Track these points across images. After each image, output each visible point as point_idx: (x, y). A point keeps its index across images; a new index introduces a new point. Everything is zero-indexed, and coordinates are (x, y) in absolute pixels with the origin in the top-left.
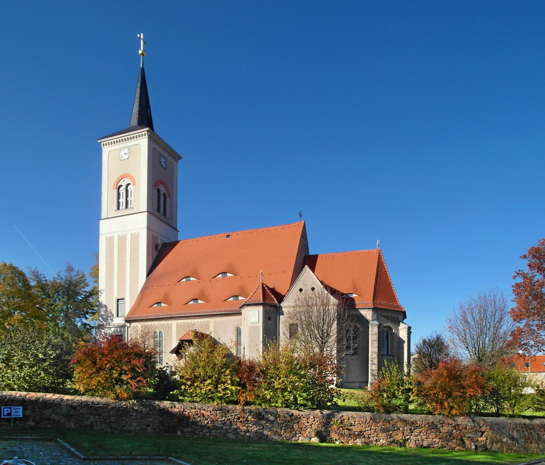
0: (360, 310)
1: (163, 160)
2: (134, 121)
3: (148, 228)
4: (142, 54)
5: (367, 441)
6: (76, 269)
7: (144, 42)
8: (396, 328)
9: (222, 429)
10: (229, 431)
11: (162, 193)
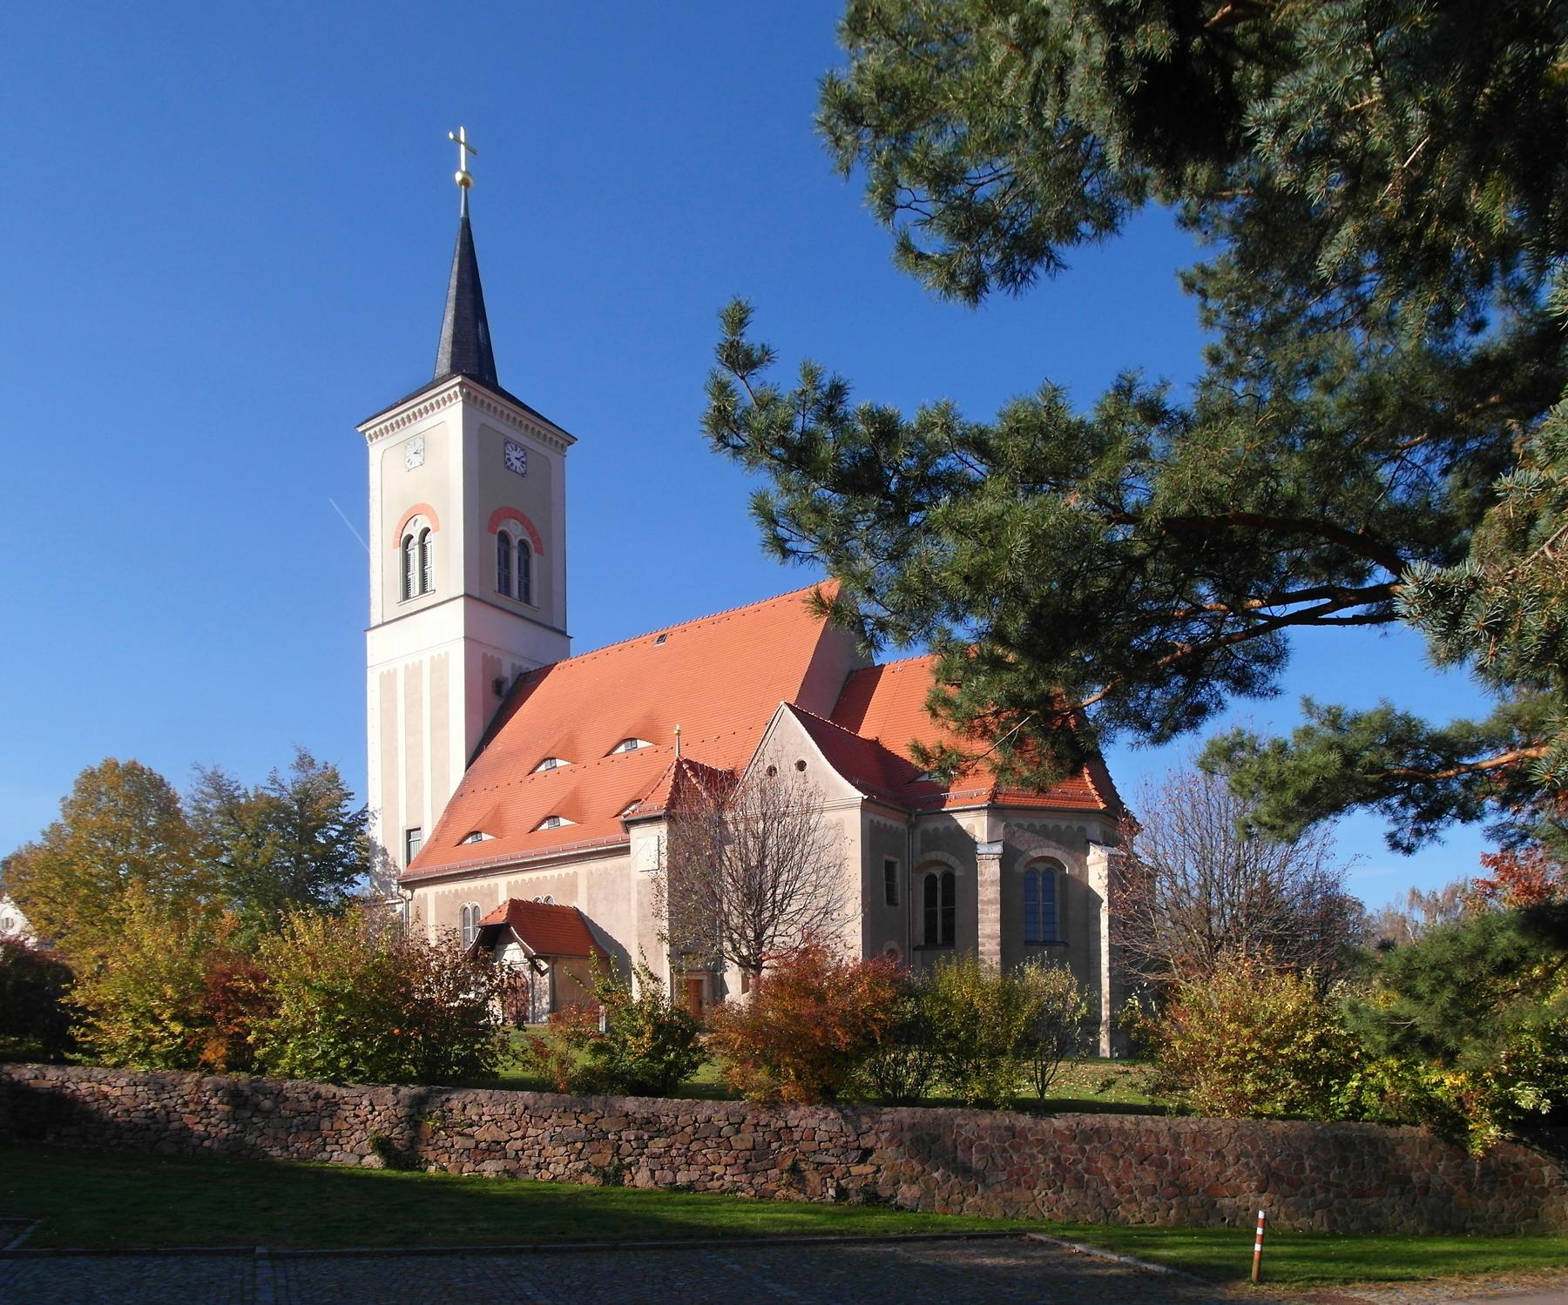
0: (955, 816)
1: (514, 455)
2: (444, 362)
3: (469, 639)
4: (465, 182)
5: (512, 1165)
6: (319, 763)
8: (1077, 860)
9: (148, 1129)
11: (515, 542)
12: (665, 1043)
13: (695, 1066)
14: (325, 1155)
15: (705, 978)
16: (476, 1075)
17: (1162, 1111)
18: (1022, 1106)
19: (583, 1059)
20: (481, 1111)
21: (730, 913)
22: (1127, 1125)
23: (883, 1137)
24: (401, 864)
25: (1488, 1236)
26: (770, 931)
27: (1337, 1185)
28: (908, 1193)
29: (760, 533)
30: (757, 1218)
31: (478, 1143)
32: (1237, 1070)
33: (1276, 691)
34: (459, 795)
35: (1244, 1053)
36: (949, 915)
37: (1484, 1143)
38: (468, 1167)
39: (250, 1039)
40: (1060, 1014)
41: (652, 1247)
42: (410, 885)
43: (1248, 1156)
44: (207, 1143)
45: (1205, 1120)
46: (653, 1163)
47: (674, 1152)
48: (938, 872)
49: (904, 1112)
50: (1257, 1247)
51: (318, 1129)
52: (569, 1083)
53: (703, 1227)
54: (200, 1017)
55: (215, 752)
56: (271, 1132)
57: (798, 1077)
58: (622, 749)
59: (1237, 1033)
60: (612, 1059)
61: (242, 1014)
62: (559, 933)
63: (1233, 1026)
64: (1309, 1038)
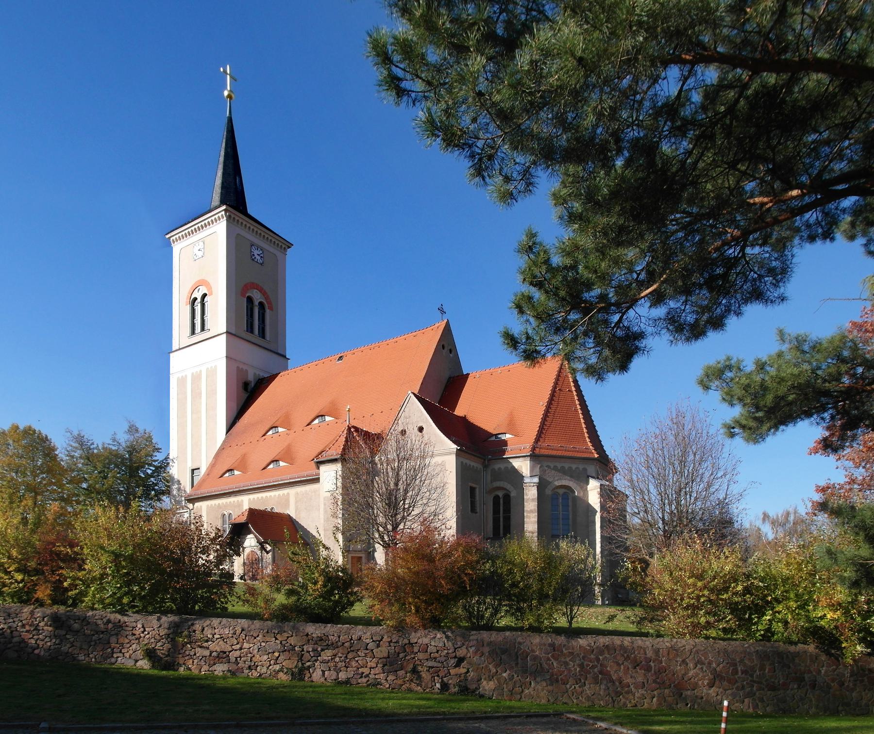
0: (511, 460)
1: (256, 252)
3: (228, 358)
4: (229, 96)
5: (233, 667)
6: (141, 430)
7: (231, 77)
10: (9, 646)
11: (256, 303)
12: (333, 589)
13: (352, 604)
14: (113, 660)
15: (363, 555)
16: (213, 609)
17: (646, 635)
18: (559, 631)
19: (281, 599)
20: (215, 632)
21: (378, 515)
22: (626, 643)
23: (472, 650)
24: (188, 489)
25: (853, 715)
26: (401, 526)
27: (758, 683)
28: (488, 686)
29: (379, 73)
30: (390, 704)
31: (211, 653)
32: (694, 608)
33: (783, 299)
34: (222, 448)
35: (698, 598)
36: (507, 519)
37: (853, 656)
38: (205, 668)
39: (65, 584)
40: (582, 571)
41: (318, 724)
42: (192, 500)
43: (703, 664)
44: (36, 652)
45: (675, 640)
46: (324, 667)
47: (337, 659)
48: (501, 494)
49: (485, 635)
50: (723, 725)
51: (109, 643)
52: (271, 614)
53: (353, 709)
54: (35, 569)
55: (78, 420)
56: (78, 644)
57: (417, 611)
58: (316, 421)
59: (695, 585)
60: (299, 599)
61: (63, 568)
62: (271, 525)
63: (690, 581)
64: (740, 588)
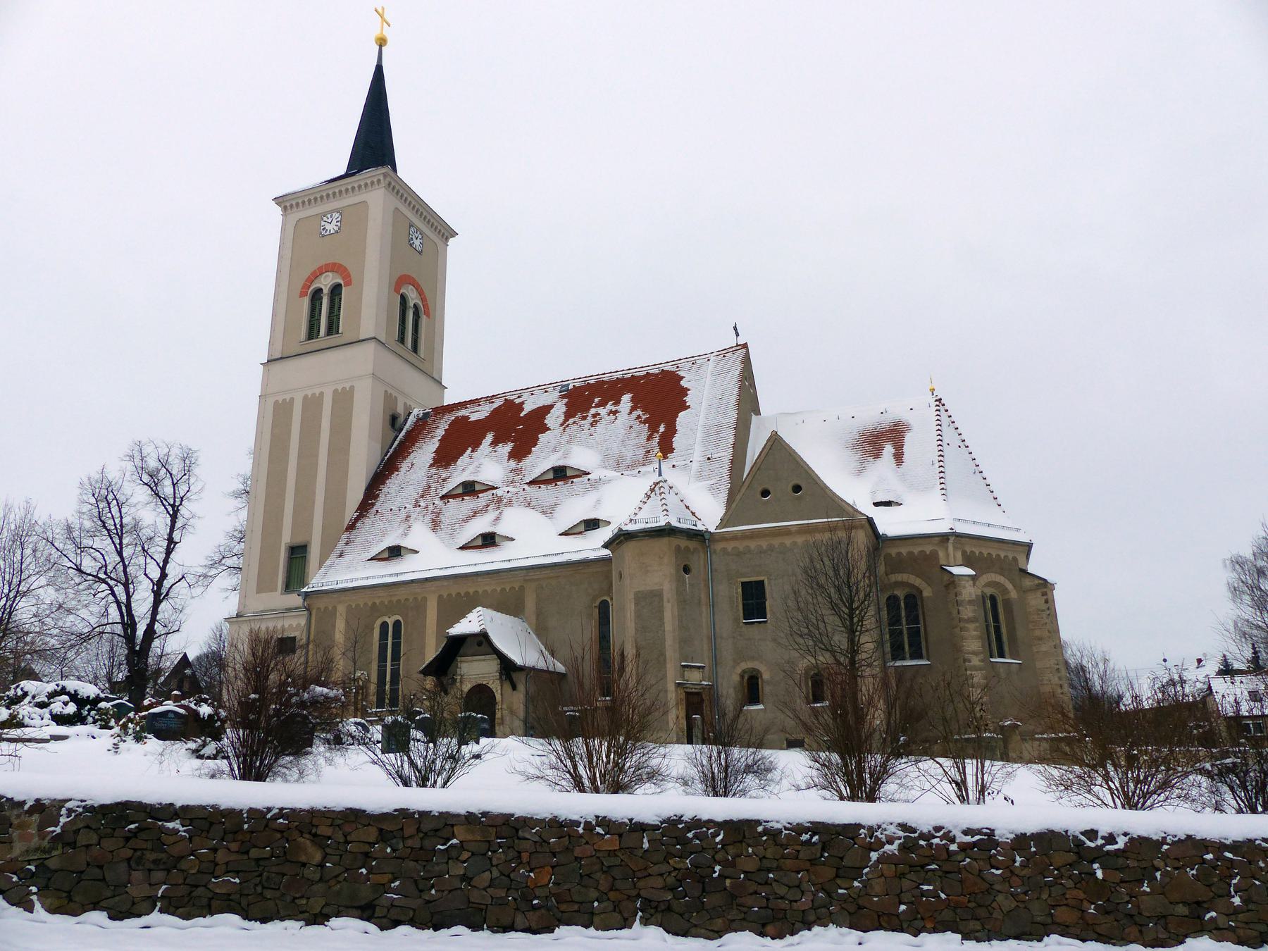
48: (900, 593)
